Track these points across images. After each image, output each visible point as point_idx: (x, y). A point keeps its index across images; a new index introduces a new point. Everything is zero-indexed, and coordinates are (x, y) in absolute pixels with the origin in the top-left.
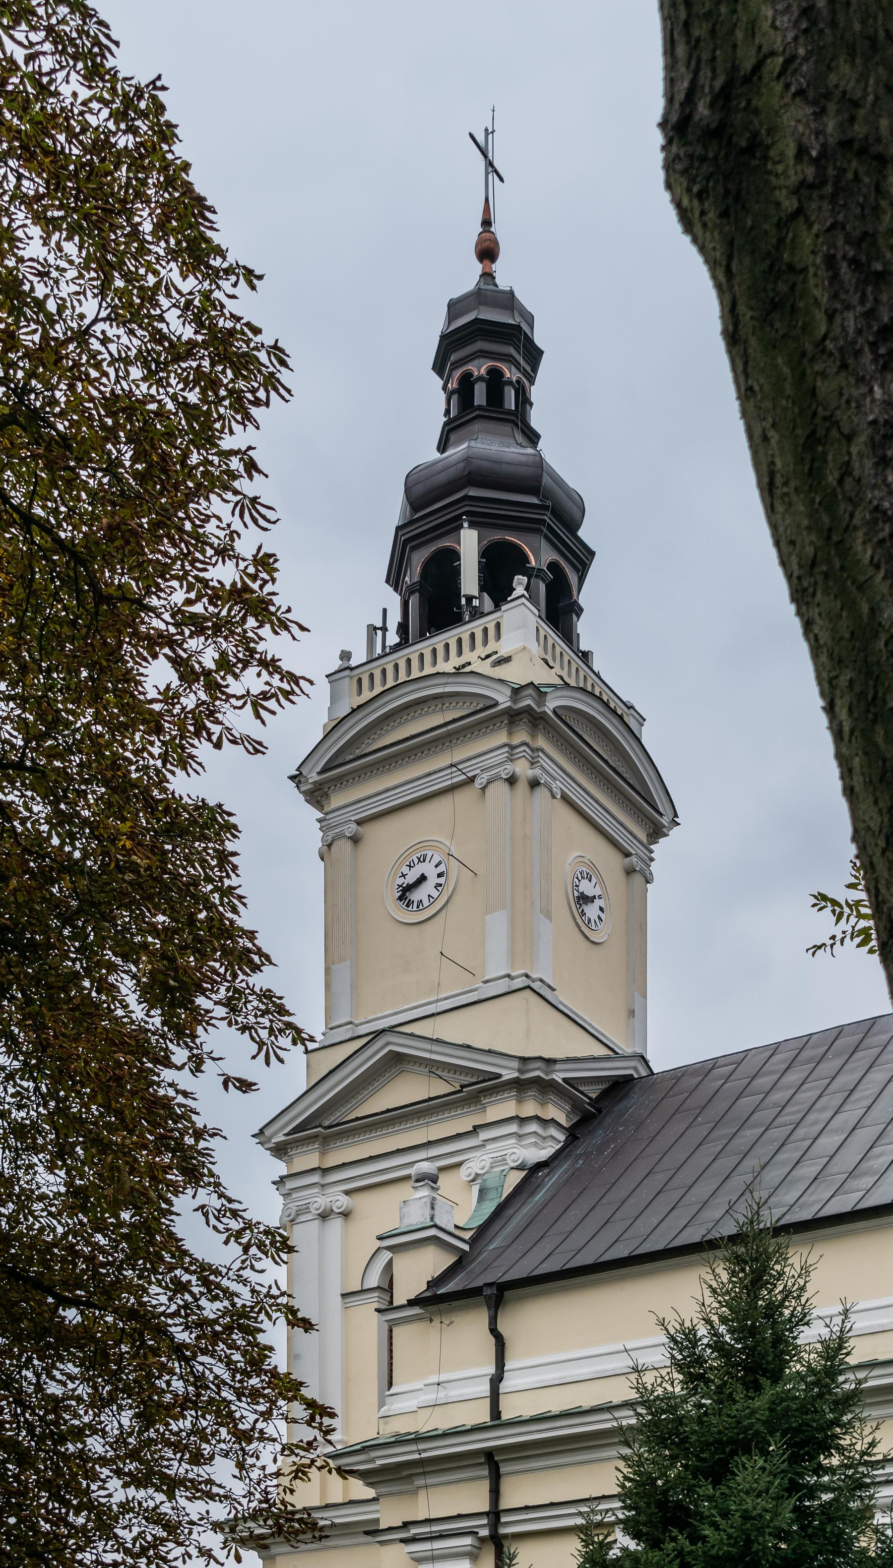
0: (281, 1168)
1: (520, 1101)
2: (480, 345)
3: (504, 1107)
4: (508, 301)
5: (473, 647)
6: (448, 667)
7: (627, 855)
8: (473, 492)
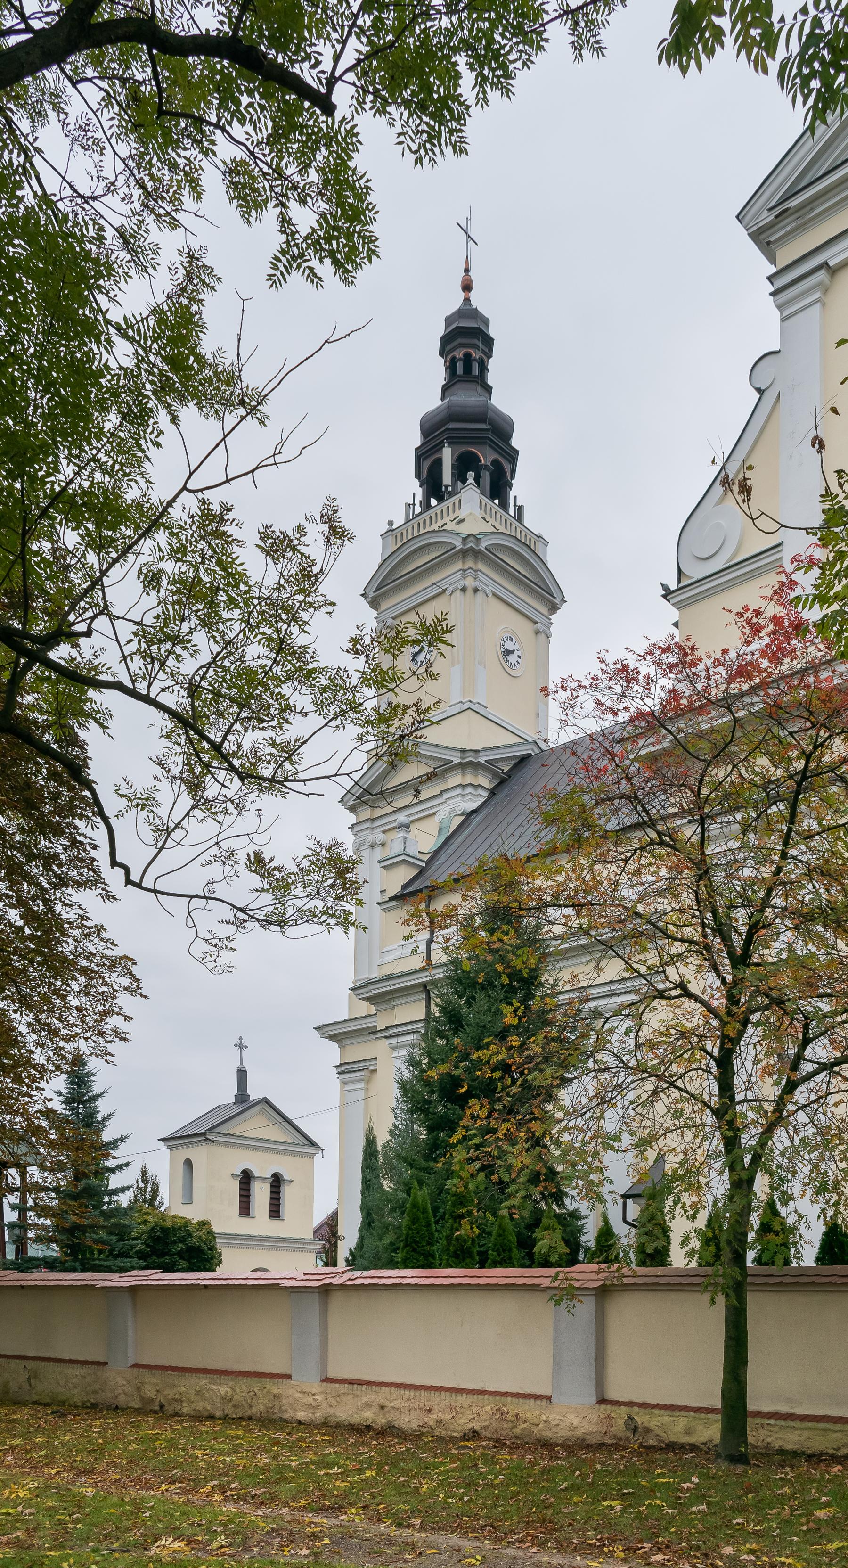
0: (352, 818)
1: (463, 775)
2: (459, 341)
3: (455, 779)
4: (475, 314)
5: (448, 515)
6: (435, 527)
7: (536, 623)
8: (452, 426)
